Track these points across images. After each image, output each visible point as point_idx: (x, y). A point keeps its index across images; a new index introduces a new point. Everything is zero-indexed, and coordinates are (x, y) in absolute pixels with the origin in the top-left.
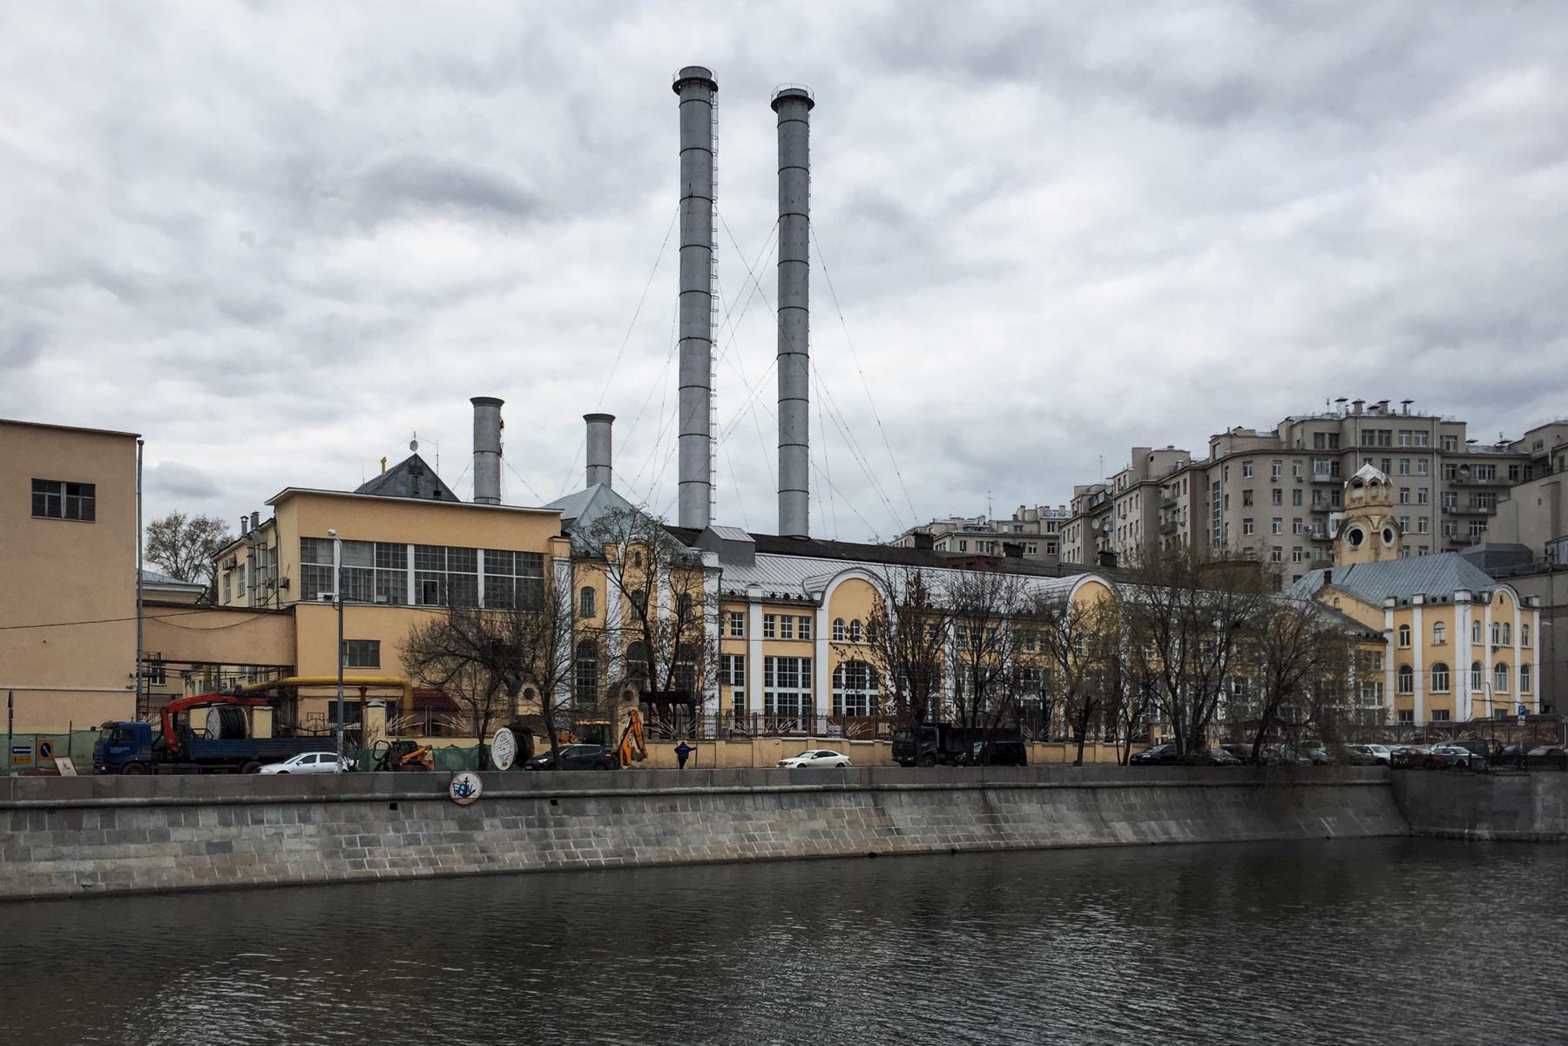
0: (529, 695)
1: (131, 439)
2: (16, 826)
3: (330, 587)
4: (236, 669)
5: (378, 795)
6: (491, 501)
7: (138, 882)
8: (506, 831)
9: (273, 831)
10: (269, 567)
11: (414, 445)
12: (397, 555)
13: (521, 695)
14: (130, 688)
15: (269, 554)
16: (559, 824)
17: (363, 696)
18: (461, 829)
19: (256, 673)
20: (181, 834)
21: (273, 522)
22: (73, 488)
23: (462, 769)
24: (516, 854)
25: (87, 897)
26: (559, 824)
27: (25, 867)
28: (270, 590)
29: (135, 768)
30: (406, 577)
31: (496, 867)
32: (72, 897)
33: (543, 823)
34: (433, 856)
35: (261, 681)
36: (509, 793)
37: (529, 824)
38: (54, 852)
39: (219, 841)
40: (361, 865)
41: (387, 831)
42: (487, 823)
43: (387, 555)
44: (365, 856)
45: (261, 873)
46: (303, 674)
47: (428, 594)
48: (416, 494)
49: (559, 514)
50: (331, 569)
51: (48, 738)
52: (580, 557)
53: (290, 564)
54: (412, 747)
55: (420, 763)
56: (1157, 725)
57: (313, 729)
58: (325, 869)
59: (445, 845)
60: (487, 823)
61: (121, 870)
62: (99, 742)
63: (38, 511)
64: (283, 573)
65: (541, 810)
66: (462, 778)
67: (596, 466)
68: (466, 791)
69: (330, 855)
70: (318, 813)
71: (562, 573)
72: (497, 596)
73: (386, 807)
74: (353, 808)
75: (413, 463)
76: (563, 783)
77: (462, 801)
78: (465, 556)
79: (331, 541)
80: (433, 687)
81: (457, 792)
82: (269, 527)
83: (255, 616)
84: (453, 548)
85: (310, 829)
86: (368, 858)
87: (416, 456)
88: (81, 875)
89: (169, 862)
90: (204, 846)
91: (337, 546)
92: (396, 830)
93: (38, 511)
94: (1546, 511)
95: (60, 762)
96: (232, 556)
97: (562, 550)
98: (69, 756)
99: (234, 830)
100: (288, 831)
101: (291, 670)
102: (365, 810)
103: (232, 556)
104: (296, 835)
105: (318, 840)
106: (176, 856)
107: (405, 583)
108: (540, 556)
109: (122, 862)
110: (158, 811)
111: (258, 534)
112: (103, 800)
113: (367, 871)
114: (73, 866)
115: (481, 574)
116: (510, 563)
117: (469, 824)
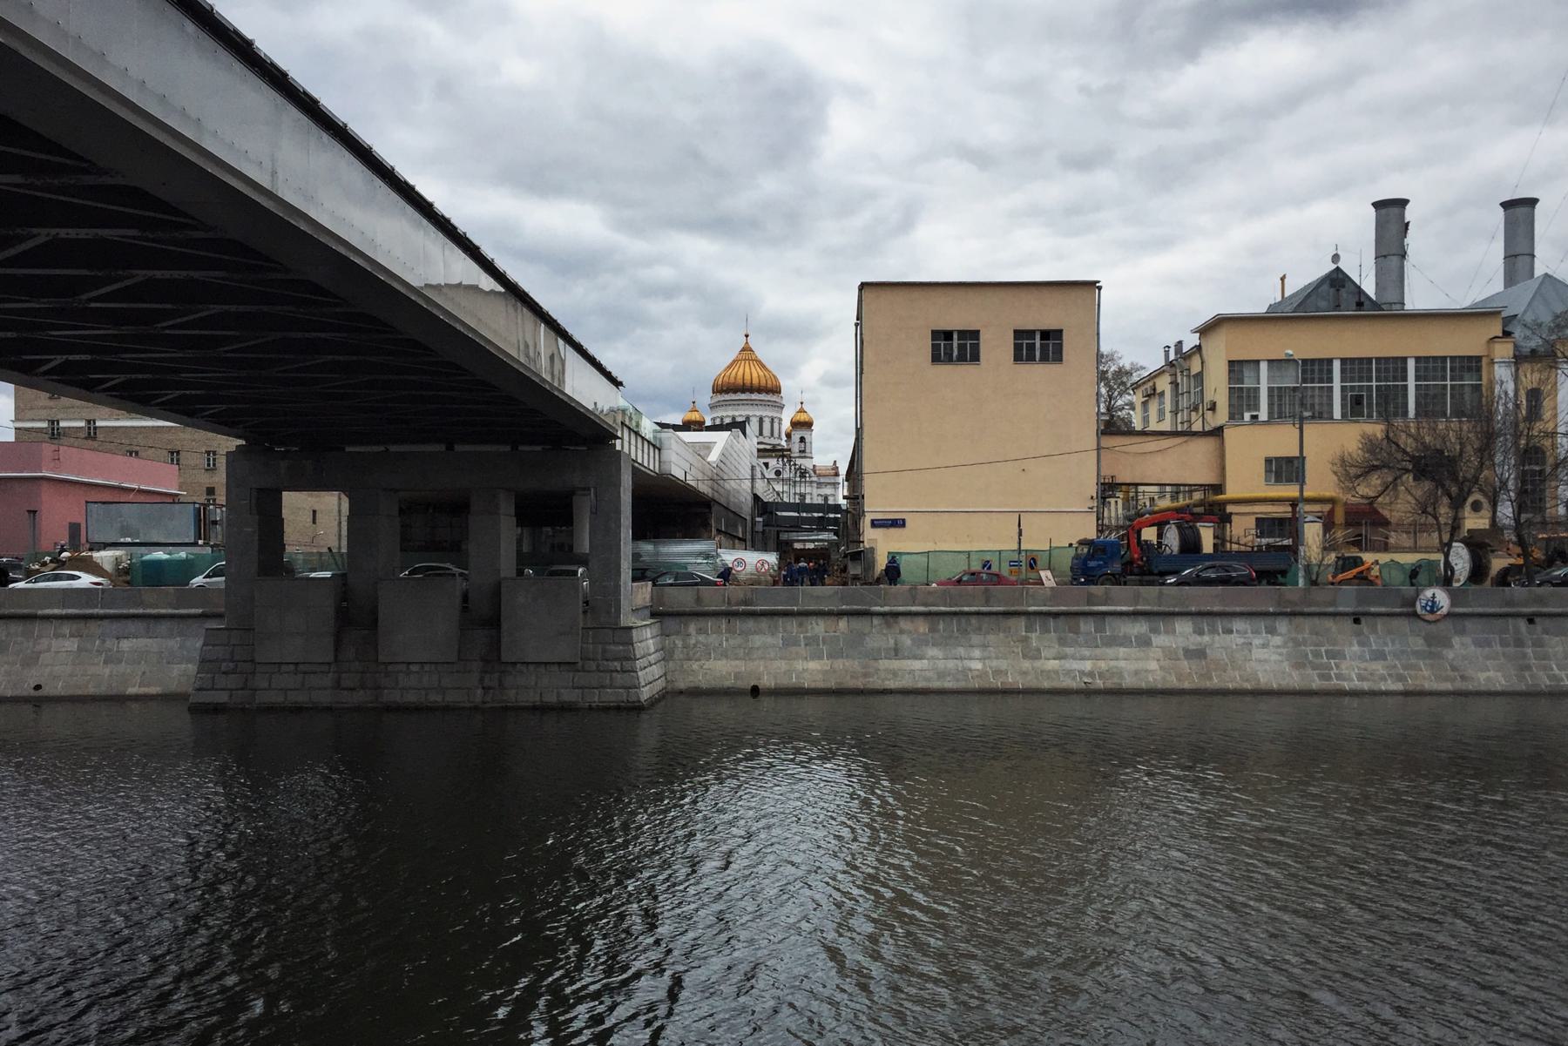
0: (1476, 507)
1: (1092, 286)
2: (1029, 629)
3: (1257, 407)
4: (1156, 489)
5: (1341, 609)
6: (1394, 307)
7: (1129, 682)
8: (1479, 650)
9: (1242, 640)
10: (1192, 391)
11: (1336, 258)
12: (1354, 369)
13: (1468, 508)
14: (1092, 508)
15: (1192, 379)
16: (1538, 643)
17: (1294, 511)
18: (1429, 645)
19: (1177, 493)
20: (1160, 640)
21: (1198, 348)
22: (1046, 335)
23: (1430, 585)
24: (1491, 674)
25: (1088, 693)
26: (1538, 643)
27: (1038, 664)
28: (1193, 414)
29: (1107, 580)
30: (1332, 391)
31: (1471, 687)
32: (1078, 692)
33: (1519, 643)
34: (1401, 671)
35: (1184, 500)
36: (1480, 610)
37: (1504, 644)
38: (1059, 653)
39: (1195, 648)
40: (1329, 678)
41: (1351, 645)
42: (1456, 641)
43: (1313, 371)
44: (1332, 669)
45: (1233, 680)
46: (1231, 492)
47: (1355, 407)
48: (1337, 307)
49: (1499, 312)
50: (1257, 390)
51: (1035, 553)
52: (1526, 357)
53: (1217, 386)
54: (1357, 562)
55: (1366, 578)
56: (450, 448)
57: (1250, 544)
58: (1294, 680)
59: (1413, 661)
60: (1456, 641)
61: (1115, 670)
62: (1076, 557)
63: (1018, 358)
64: (1208, 397)
65: (1517, 631)
66: (1429, 593)
67: (1516, 256)
68: (1433, 606)
69: (1298, 665)
70: (1282, 625)
71: (1503, 373)
72: (1429, 405)
73: (1350, 621)
74: (1316, 620)
75: (1335, 276)
76: (1540, 600)
77: (1430, 617)
78: (1396, 366)
79: (1257, 362)
80: (1367, 502)
81: (1424, 608)
82: (1194, 353)
83: (1185, 439)
84: (1456, 357)
85: (1277, 640)
86: (1335, 671)
87: (1338, 269)
88: (1082, 673)
89: (1153, 665)
90: (1181, 652)
91: (1264, 366)
92: (1361, 644)
93: (936, 359)
94: (1103, 463)
95: (1043, 574)
96: (1151, 384)
97: (1504, 351)
98: (1049, 569)
99: (1206, 638)
100: (1257, 641)
101: (1218, 488)
102: (1329, 623)
103: (1151, 384)
104: (1264, 646)
105: (1284, 651)
106: (1158, 660)
107: (1330, 398)
108: (1479, 359)
109: (1113, 663)
110: (1140, 618)
111: (1180, 362)
112: (1096, 608)
113: (1334, 683)
114: (1076, 665)
115: (1411, 383)
116: (1444, 369)
117: (1437, 642)
